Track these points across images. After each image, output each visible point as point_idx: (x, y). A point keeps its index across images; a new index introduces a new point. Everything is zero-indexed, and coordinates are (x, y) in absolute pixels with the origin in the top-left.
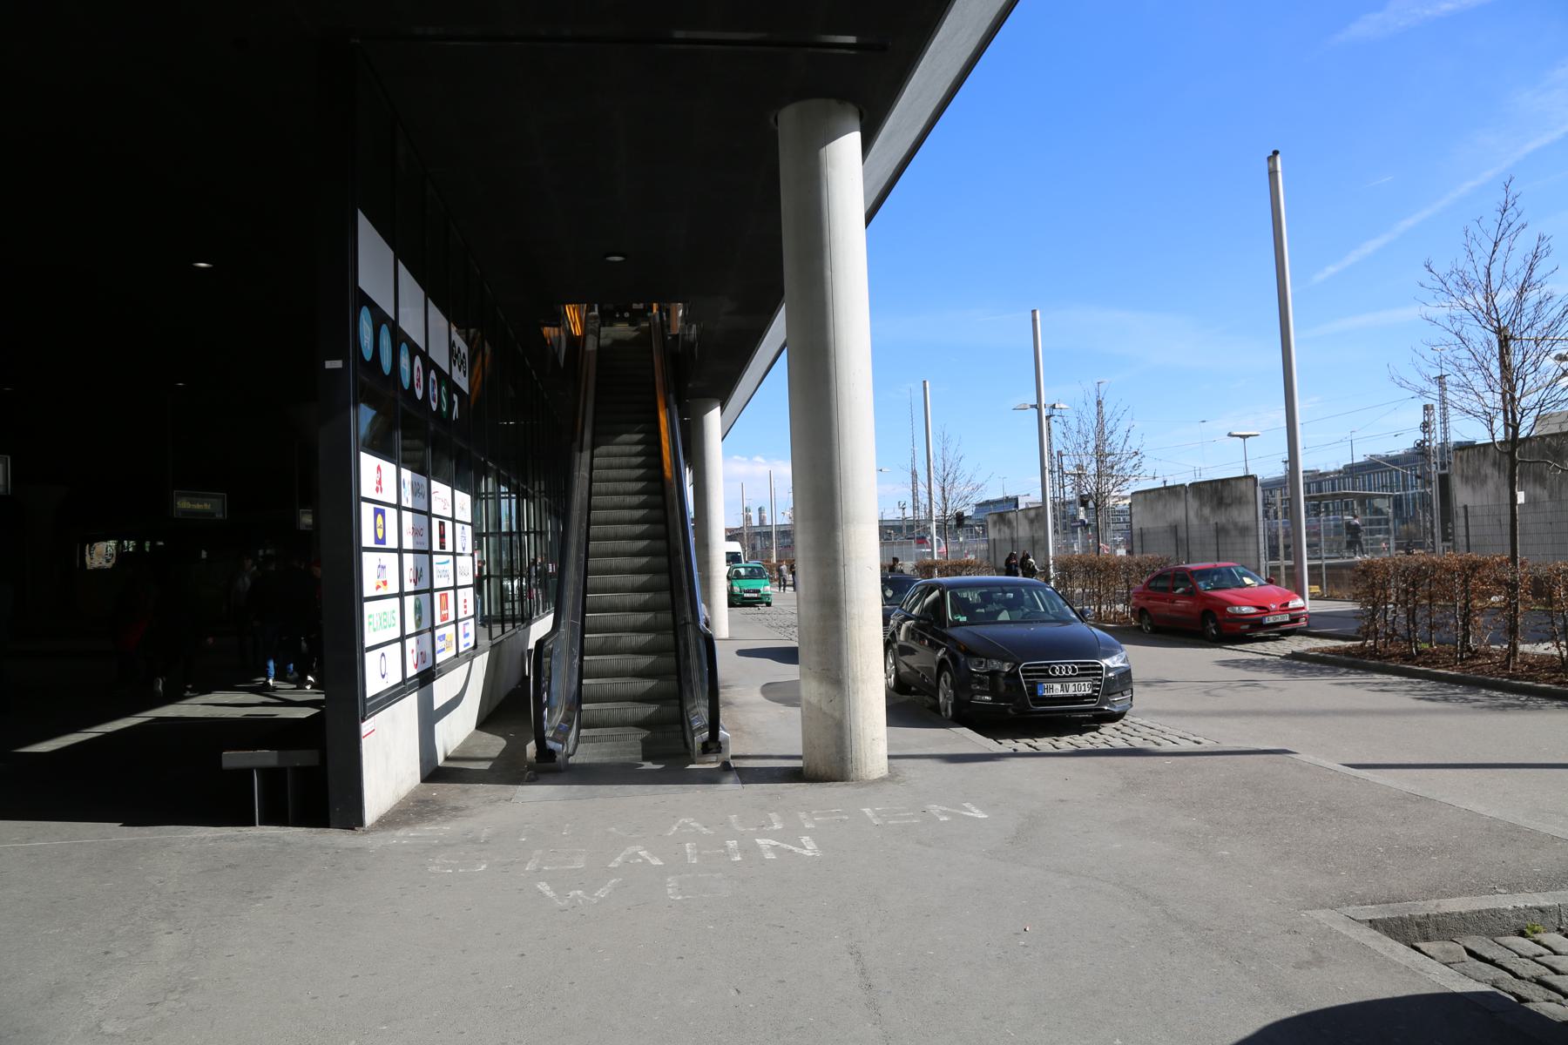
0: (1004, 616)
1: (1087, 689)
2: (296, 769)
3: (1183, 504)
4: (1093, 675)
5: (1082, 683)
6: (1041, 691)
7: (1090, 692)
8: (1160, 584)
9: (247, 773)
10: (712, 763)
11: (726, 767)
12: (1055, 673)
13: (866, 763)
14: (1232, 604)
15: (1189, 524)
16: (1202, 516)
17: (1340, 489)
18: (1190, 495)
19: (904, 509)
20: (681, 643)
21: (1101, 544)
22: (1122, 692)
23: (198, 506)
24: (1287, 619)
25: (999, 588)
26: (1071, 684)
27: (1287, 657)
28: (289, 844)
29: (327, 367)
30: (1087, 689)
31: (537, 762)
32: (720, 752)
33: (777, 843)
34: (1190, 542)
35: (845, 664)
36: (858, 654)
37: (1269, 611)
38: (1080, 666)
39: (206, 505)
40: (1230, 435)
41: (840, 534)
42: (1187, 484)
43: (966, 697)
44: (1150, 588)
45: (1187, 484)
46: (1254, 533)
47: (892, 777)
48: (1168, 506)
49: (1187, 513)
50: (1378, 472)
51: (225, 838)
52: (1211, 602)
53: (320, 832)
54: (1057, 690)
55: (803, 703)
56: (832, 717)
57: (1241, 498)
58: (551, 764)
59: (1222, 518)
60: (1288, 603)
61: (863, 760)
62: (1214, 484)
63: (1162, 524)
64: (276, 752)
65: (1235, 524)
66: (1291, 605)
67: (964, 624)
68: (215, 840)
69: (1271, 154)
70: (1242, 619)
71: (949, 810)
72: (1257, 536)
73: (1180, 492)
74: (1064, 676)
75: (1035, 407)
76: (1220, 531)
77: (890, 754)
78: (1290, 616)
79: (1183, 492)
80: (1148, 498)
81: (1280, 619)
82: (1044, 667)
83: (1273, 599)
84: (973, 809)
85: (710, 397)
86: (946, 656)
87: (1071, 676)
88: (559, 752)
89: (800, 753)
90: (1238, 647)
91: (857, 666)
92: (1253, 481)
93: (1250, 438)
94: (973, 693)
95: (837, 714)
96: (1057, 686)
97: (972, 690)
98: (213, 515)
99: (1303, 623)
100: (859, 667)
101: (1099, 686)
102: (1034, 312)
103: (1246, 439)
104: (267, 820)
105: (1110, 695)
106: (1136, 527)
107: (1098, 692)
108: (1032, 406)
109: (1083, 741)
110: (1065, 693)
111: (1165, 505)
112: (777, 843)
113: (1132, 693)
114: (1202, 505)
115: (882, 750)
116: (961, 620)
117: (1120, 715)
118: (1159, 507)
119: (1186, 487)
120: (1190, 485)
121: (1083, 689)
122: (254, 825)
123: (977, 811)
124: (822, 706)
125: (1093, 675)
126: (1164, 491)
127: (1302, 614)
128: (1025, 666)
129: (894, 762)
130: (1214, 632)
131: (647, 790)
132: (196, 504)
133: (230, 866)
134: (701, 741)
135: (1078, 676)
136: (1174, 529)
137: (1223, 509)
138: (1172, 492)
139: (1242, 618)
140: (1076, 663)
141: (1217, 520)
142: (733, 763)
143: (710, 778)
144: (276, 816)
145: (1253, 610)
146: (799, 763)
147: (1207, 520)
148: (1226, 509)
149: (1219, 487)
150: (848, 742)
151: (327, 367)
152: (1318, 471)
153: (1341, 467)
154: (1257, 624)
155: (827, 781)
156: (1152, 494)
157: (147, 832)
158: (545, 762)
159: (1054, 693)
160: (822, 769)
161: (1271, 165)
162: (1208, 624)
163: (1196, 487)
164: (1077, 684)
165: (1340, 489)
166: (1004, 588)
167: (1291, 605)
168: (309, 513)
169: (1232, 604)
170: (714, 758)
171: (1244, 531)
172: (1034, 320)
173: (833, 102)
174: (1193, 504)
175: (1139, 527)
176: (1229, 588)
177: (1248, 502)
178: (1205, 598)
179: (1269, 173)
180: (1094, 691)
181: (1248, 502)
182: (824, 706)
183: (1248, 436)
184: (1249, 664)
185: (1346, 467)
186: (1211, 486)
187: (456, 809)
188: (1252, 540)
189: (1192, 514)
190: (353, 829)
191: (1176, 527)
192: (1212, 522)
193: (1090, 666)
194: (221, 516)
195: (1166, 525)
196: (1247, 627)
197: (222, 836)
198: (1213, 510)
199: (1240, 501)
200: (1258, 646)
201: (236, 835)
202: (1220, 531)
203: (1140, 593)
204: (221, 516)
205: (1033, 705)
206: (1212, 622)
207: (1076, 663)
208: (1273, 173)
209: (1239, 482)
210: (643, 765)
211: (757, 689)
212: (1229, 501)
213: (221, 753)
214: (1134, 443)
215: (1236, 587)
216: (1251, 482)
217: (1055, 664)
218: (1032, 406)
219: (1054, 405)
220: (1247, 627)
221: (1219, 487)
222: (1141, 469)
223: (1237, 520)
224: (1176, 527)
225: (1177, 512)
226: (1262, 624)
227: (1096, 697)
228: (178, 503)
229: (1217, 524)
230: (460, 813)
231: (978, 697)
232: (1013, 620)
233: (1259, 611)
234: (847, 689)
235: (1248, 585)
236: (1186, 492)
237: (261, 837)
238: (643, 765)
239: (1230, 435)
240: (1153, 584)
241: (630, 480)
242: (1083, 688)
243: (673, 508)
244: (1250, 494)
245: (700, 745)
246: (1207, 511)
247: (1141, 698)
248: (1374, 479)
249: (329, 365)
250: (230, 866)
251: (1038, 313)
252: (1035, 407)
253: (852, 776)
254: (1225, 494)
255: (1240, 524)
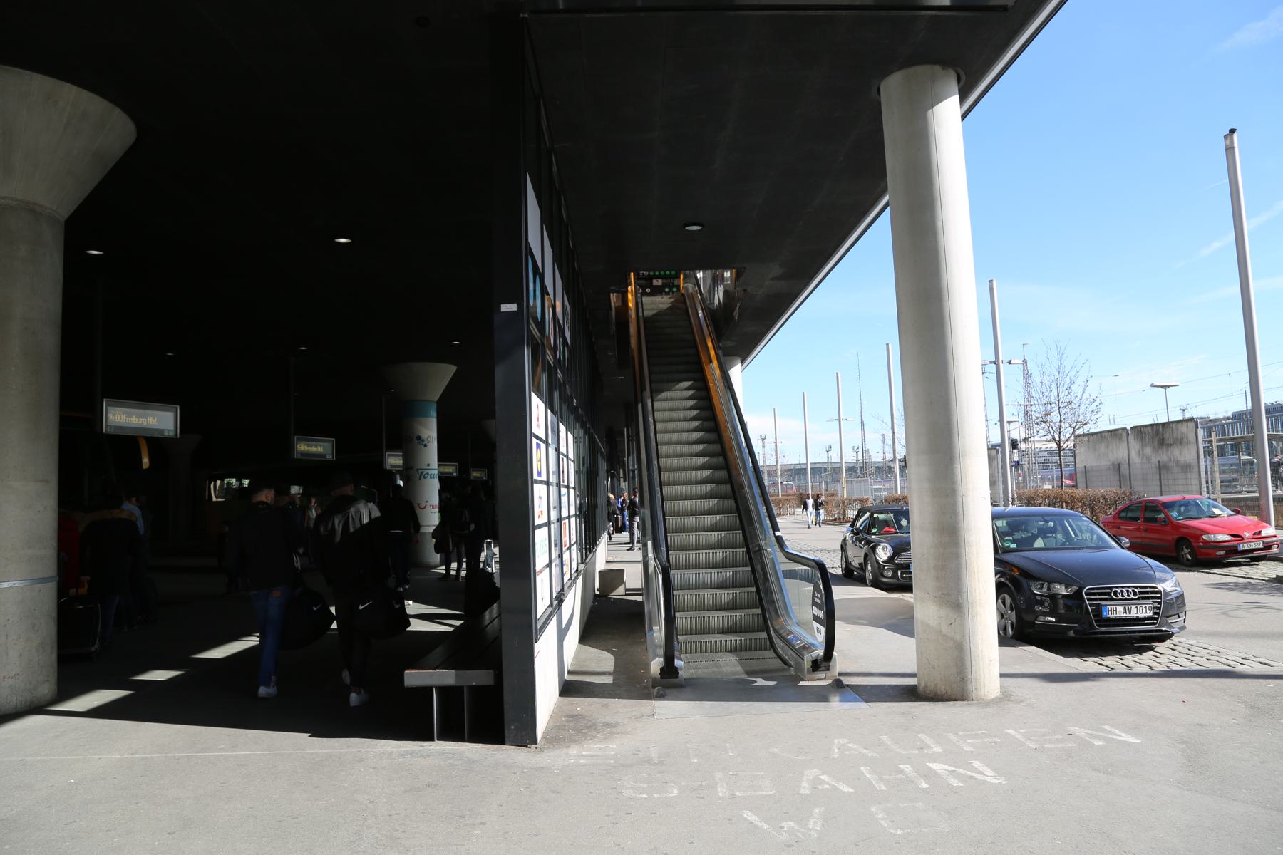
0: (1039, 543)
1: (1148, 611)
2: (471, 688)
3: (1125, 445)
4: (1152, 598)
5: (1144, 606)
6: (1105, 613)
7: (1151, 614)
8: (1130, 515)
9: (426, 691)
10: (822, 680)
11: (838, 685)
12: (1117, 596)
13: (984, 684)
14: (1207, 533)
15: (1131, 462)
16: (1143, 454)
17: (1233, 434)
18: (1131, 436)
19: (857, 452)
20: (758, 567)
21: (1064, 480)
22: (1178, 614)
23: (313, 449)
24: (1261, 546)
25: (1040, 518)
26: (1133, 607)
27: (1271, 580)
28: (473, 762)
29: (515, 305)
30: (1148, 611)
31: (662, 678)
32: (828, 670)
33: (953, 769)
34: (1132, 477)
35: (965, 590)
36: (977, 580)
37: (1243, 539)
38: (1140, 590)
39: (319, 448)
40: (1153, 386)
41: (957, 466)
42: (1129, 428)
43: (1029, 618)
44: (1120, 518)
45: (1129, 428)
46: (1196, 469)
47: (1006, 697)
48: (1110, 447)
49: (1131, 452)
50: (1271, 417)
51: (412, 753)
52: (1186, 530)
53: (497, 750)
54: (1120, 612)
55: (918, 628)
56: (952, 639)
57: (1182, 439)
58: (675, 680)
59: (1164, 456)
60: (1260, 532)
61: (982, 680)
62: (1155, 427)
63: (1104, 463)
64: (453, 671)
65: (1177, 462)
66: (1263, 534)
67: (1014, 550)
68: (403, 755)
69: (1228, 133)
70: (1218, 546)
71: (1094, 733)
72: (1199, 472)
73: (1121, 435)
74: (1126, 600)
75: (994, 362)
76: (1161, 468)
77: (1003, 672)
78: (1264, 543)
79: (1125, 434)
80: (1091, 440)
81: (1253, 546)
82: (1106, 591)
83: (1246, 528)
84: (1117, 732)
85: (735, 355)
86: (1003, 580)
87: (1132, 599)
88: (681, 669)
89: (912, 668)
90: (1215, 571)
91: (975, 590)
92: (1193, 424)
93: (864, 419)
94: (1037, 614)
95: (957, 637)
96: (1121, 609)
97: (1035, 612)
98: (325, 456)
99: (1275, 550)
100: (977, 591)
101: (1159, 608)
102: (991, 281)
103: (1167, 389)
104: (447, 735)
105: (1168, 617)
106: (1080, 465)
107: (1158, 614)
108: (991, 362)
109: (1132, 661)
110: (1128, 615)
111: (1108, 447)
112: (953, 769)
113: (1185, 615)
114: (1143, 446)
115: (996, 671)
116: (1011, 547)
117: (1170, 636)
118: (1102, 447)
119: (1128, 430)
120: (1132, 428)
121: (1144, 611)
122: (433, 740)
123: (1124, 735)
124: (943, 629)
125: (1152, 598)
126: (1106, 434)
127: (1275, 541)
128: (1088, 589)
129: (1003, 679)
130: (1190, 558)
131: (778, 708)
132: (311, 447)
133: (429, 785)
134: (811, 659)
135: (1139, 599)
136: (1117, 467)
137: (1165, 450)
138: (1115, 434)
139: (1218, 545)
140: (1136, 587)
141: (1159, 458)
142: (846, 680)
143: (821, 695)
144: (452, 732)
145: (1228, 538)
146: (912, 681)
147: (1149, 460)
148: (1167, 450)
149: (1161, 429)
150: (968, 664)
151: (515, 305)
152: (1209, 417)
153: (1230, 414)
154: (1234, 551)
155: (947, 700)
156: (1095, 436)
157: (336, 744)
158: (666, 678)
159: (1118, 615)
160: (942, 688)
161: (1228, 142)
162: (1183, 550)
163: (1139, 431)
164: (1138, 606)
165: (1233, 434)
166: (1045, 517)
167: (1263, 534)
168: (399, 456)
169: (1207, 533)
170: (822, 675)
171: (1186, 468)
172: (991, 289)
173: (937, 68)
174: (1135, 445)
175: (1157, 460)
176: (1201, 518)
177: (1189, 443)
178: (1177, 527)
179: (1226, 150)
180: (1155, 613)
181: (1189, 443)
182: (945, 629)
183: (1169, 387)
184: (1239, 587)
185: (1234, 414)
186: (1153, 430)
187: (607, 725)
188: (1195, 475)
189: (1134, 454)
190: (526, 746)
191: (1119, 464)
192: (1154, 460)
193: (1149, 589)
194: (331, 457)
195: (1108, 463)
196: (1222, 553)
197: (406, 751)
198: (1154, 448)
199: (1181, 442)
200: (1235, 570)
201: (420, 751)
202: (1161, 468)
203: (1109, 522)
204: (331, 457)
205: (1097, 626)
206: (1187, 548)
207: (1136, 587)
208: (1230, 150)
209: (1179, 425)
210: (756, 682)
211: (1187, 629)
212: (1171, 442)
213: (403, 672)
214: (1092, 390)
215: (1206, 517)
216: (1191, 425)
217: (1117, 587)
218: (991, 362)
219: (1011, 361)
220: (1222, 553)
221: (1161, 429)
222: (1100, 414)
223: (1179, 459)
224: (1119, 464)
225: (1119, 452)
226: (1237, 550)
227: (1157, 619)
228: (298, 446)
229: (1159, 462)
230: (614, 730)
231: (1042, 618)
232: (1048, 546)
233: (1234, 539)
234: (966, 613)
235: (1218, 516)
236: (1128, 435)
237: (443, 753)
238: (756, 682)
239: (1153, 386)
240: (1123, 514)
241: (685, 420)
242: (1144, 610)
243: (732, 448)
244: (1192, 436)
245: (810, 664)
246: (1148, 451)
247: (1193, 619)
248: (1237, 428)
249: (505, 308)
250: (429, 785)
251: (994, 283)
252: (994, 362)
253: (972, 695)
254: (1166, 436)
255: (1183, 462)
